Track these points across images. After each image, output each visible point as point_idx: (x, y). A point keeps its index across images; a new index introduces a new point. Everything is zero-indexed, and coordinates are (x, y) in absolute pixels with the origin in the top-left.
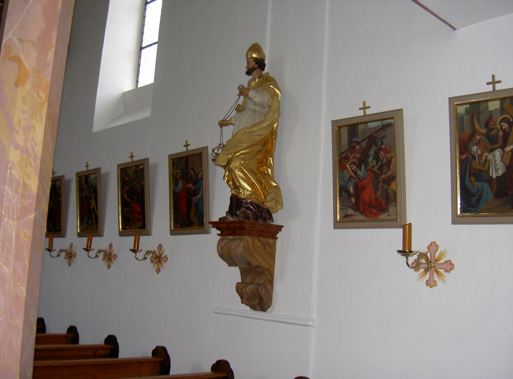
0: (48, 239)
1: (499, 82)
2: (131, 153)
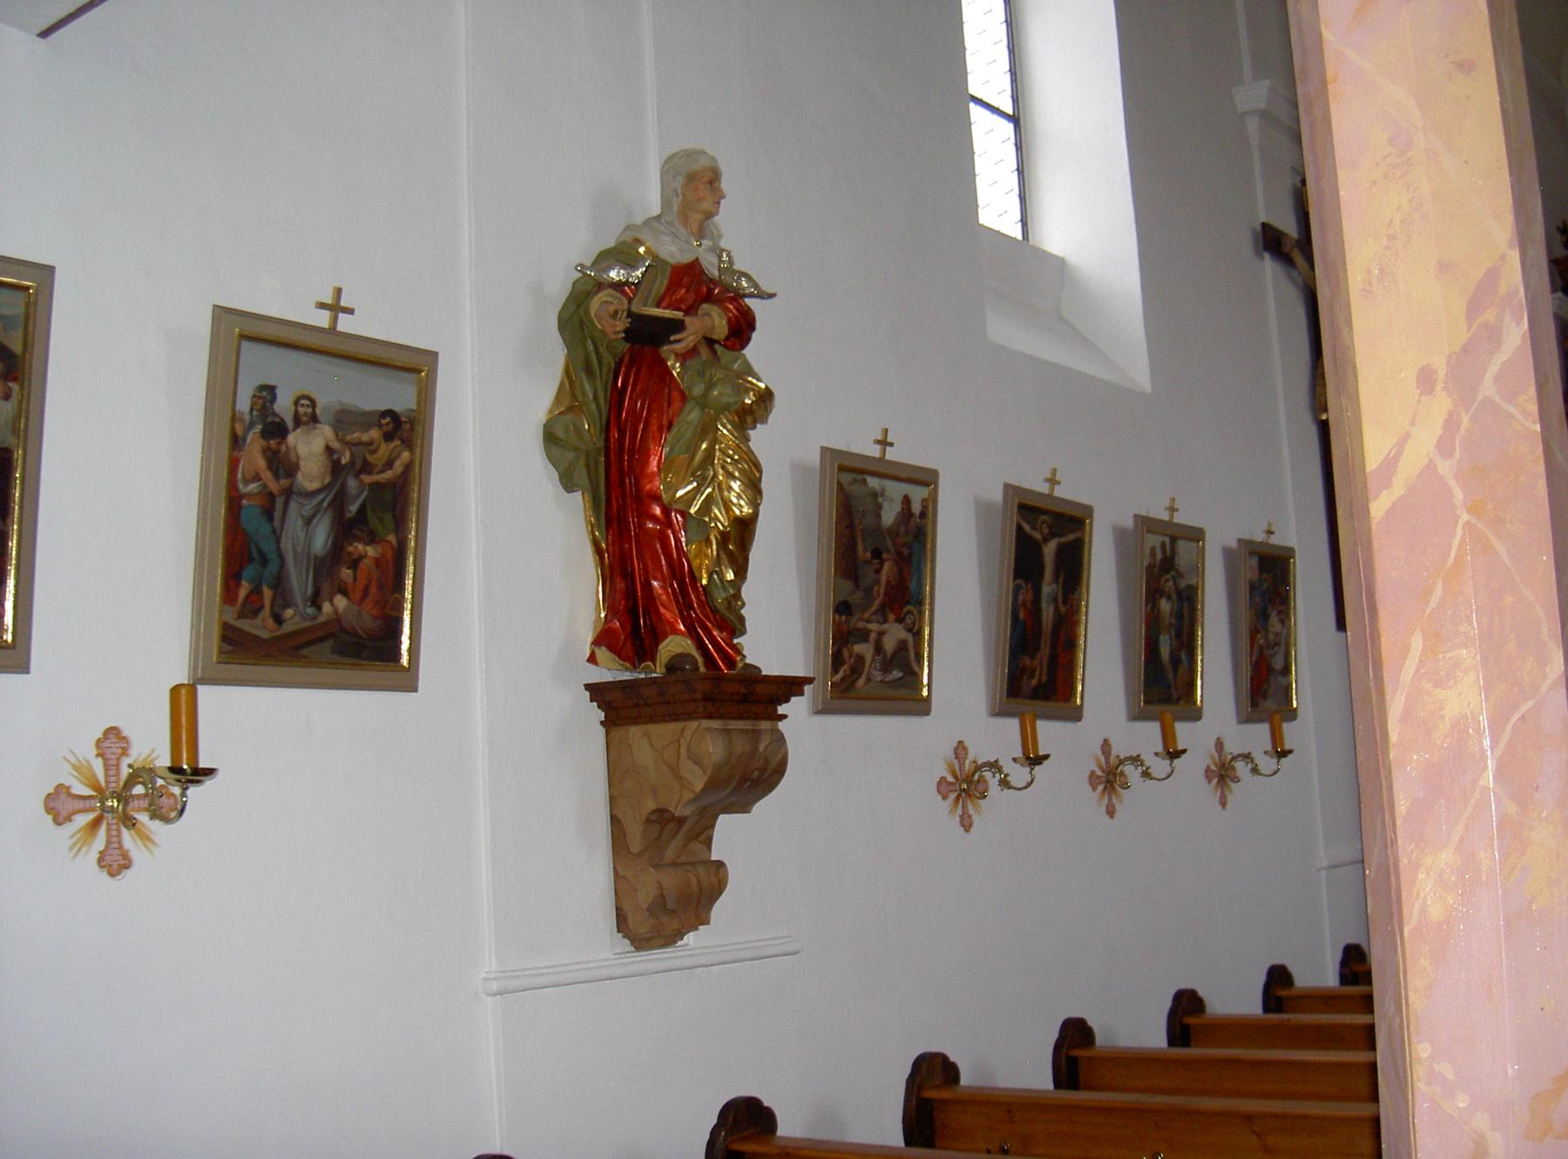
0: (1014, 724)
1: (350, 311)
2: (1173, 500)
